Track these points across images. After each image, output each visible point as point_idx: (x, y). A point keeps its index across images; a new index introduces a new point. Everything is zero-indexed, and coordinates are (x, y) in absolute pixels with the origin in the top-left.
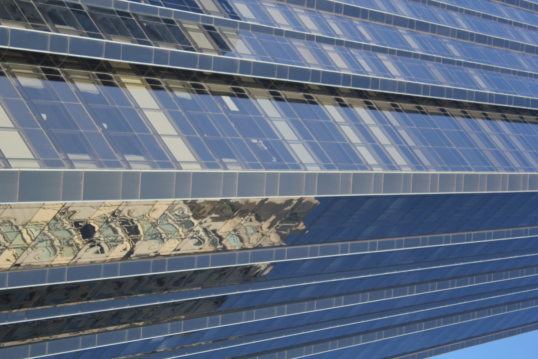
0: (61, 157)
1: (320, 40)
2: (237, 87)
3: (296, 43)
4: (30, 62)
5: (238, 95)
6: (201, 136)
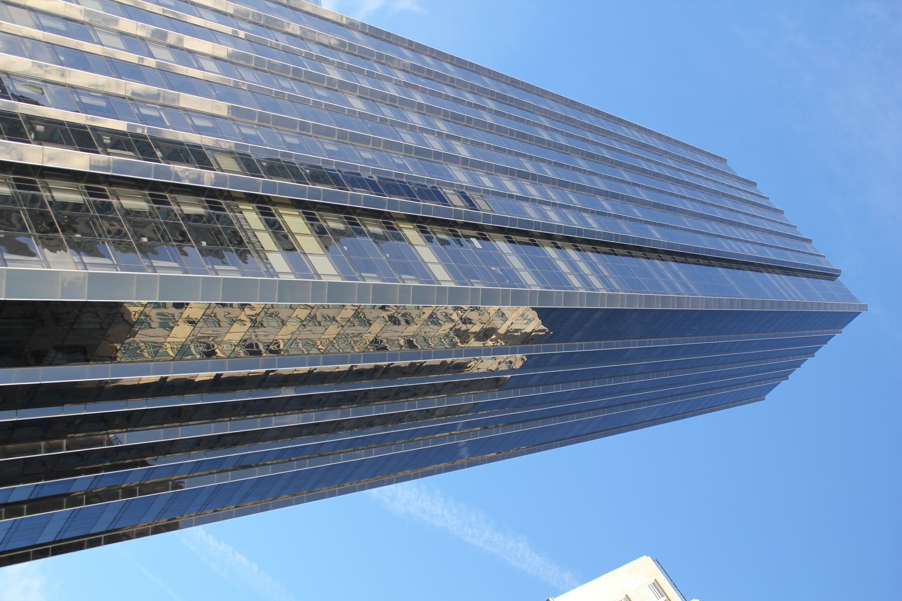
0: (357, 275)
1: (541, 202)
2: (482, 232)
3: (524, 204)
4: (336, 212)
5: (482, 238)
6: (135, 241)
